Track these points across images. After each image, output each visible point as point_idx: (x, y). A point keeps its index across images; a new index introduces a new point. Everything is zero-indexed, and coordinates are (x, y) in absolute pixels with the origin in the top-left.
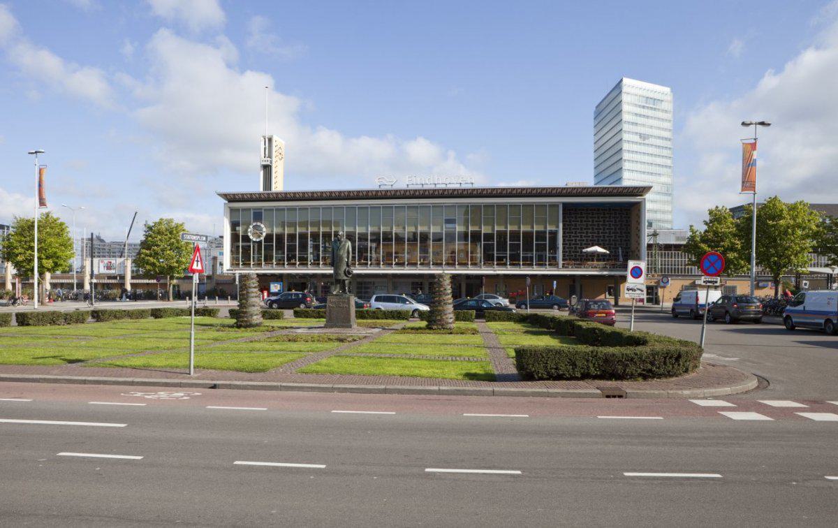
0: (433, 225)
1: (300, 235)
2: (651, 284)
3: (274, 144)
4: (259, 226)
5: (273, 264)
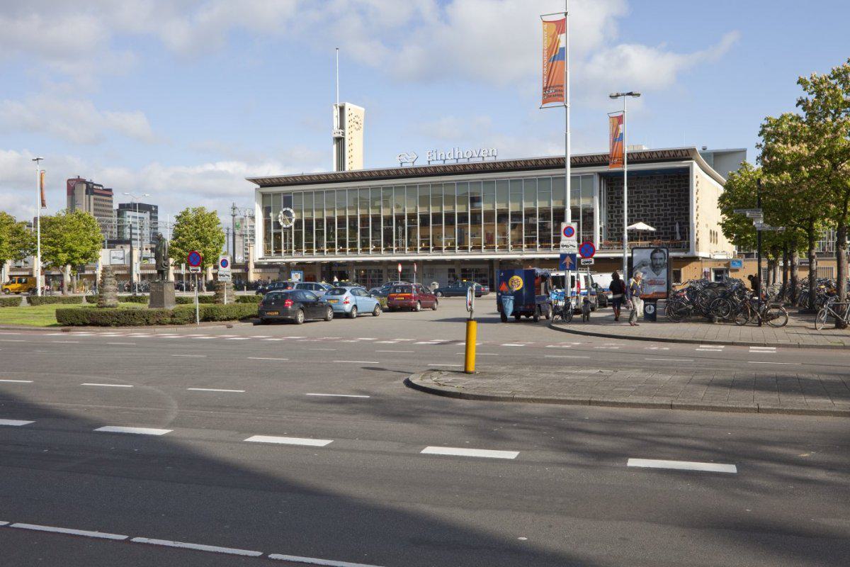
0: (582, 197)
1: (409, 215)
2: (720, 267)
3: (347, 112)
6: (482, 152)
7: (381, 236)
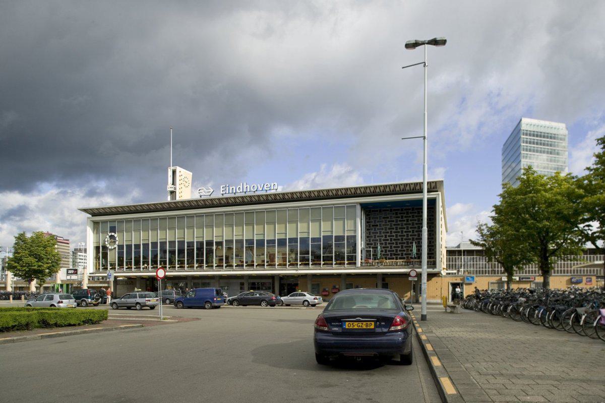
4: (114, 236)
6: (265, 186)
7: (184, 255)
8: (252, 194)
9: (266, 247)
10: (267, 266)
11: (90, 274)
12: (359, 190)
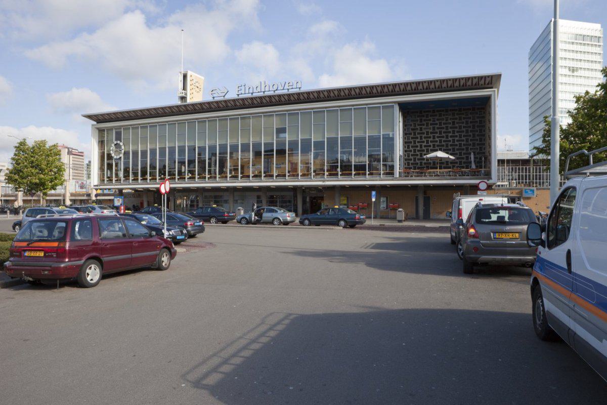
4: (119, 144)
5: (129, 179)
6: (287, 85)
8: (271, 93)
9: (287, 155)
10: (289, 176)
11: (94, 186)
12: (375, 89)
